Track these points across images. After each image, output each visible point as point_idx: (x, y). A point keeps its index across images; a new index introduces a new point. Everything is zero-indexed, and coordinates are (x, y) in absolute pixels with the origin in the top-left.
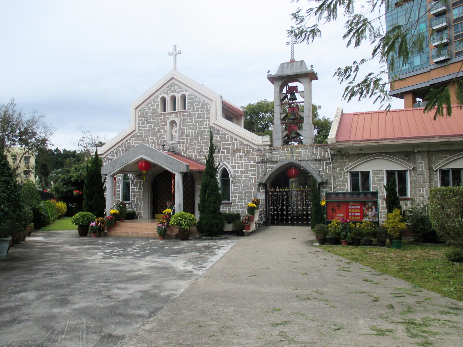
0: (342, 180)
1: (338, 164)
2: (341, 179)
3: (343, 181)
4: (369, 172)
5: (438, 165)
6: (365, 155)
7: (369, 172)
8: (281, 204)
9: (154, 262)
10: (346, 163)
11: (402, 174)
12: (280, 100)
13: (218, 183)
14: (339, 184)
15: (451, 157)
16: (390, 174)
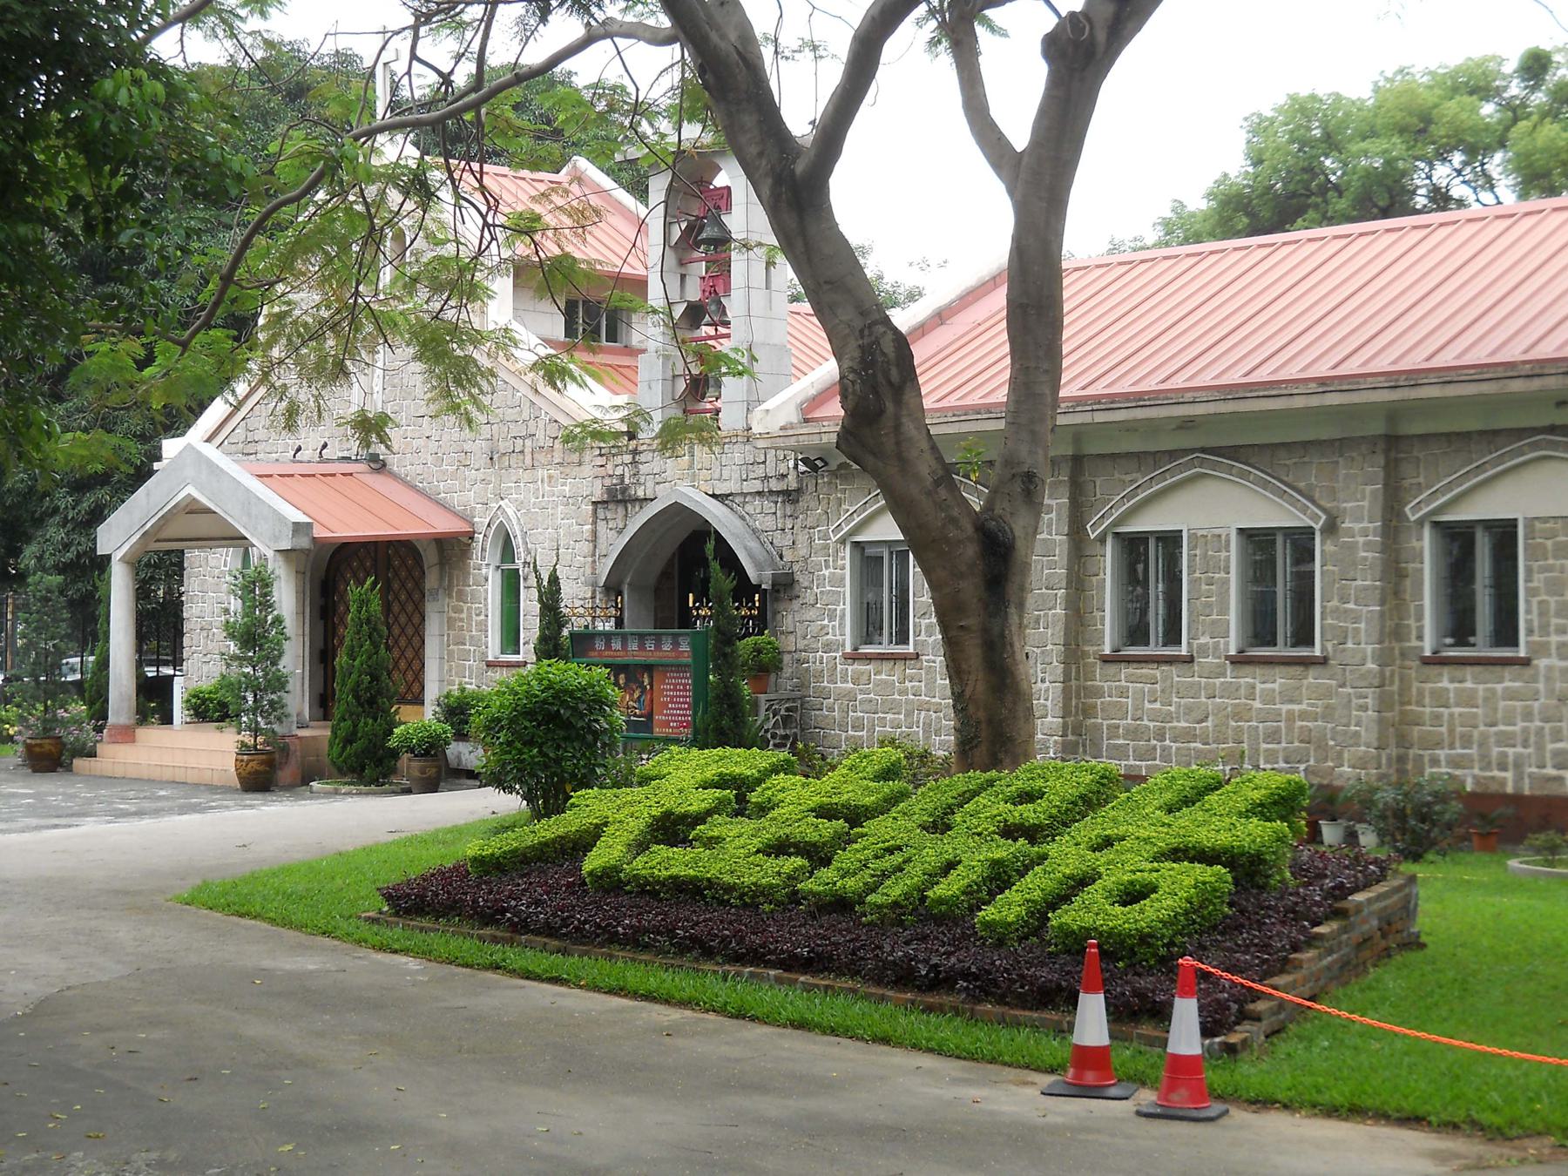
4: (1516, 520)
5: (1103, 516)
6: (1492, 437)
9: (483, 550)
11: (1301, 542)
15: (1144, 483)
16: (1257, 541)
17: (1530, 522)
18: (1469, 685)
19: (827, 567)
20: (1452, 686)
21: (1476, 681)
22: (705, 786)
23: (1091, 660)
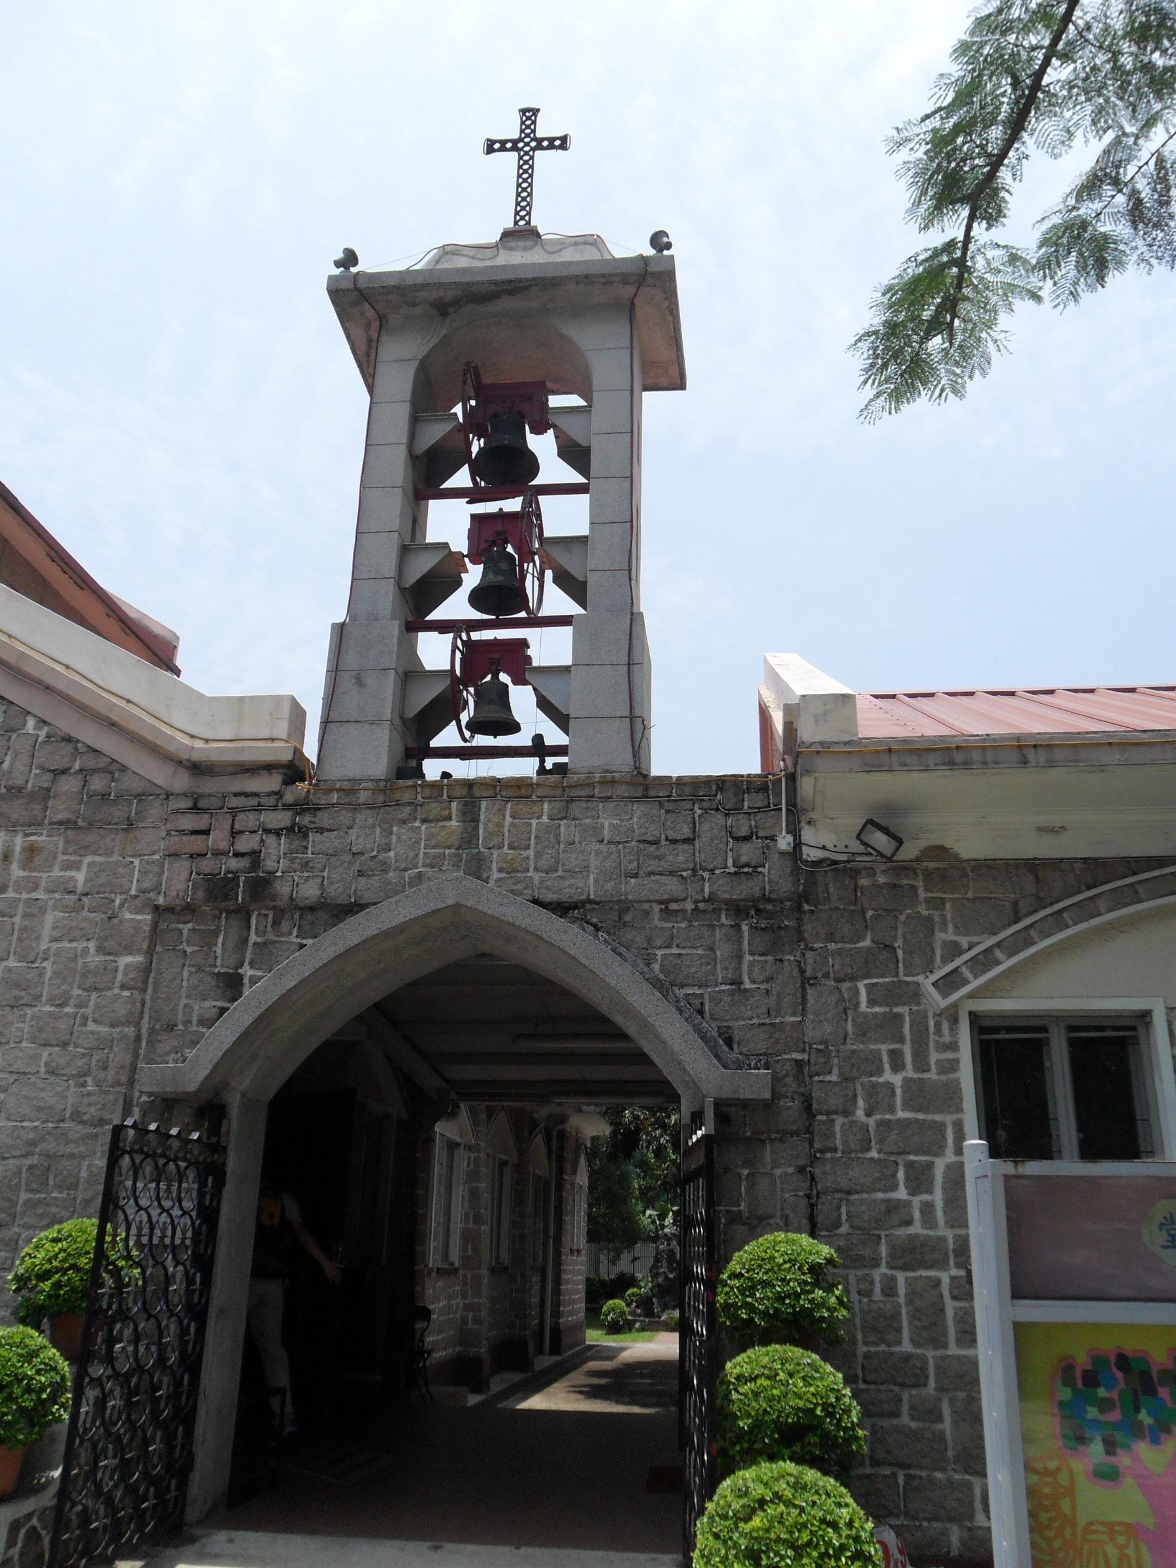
0: (906, 1081)
1: (867, 943)
2: (897, 1080)
3: (917, 1095)
4: (1144, 1016)
7: (1144, 1016)
8: (1024, 104)
10: (941, 936)
12: (413, 458)
13: (916, 1155)
14: (880, 1123)
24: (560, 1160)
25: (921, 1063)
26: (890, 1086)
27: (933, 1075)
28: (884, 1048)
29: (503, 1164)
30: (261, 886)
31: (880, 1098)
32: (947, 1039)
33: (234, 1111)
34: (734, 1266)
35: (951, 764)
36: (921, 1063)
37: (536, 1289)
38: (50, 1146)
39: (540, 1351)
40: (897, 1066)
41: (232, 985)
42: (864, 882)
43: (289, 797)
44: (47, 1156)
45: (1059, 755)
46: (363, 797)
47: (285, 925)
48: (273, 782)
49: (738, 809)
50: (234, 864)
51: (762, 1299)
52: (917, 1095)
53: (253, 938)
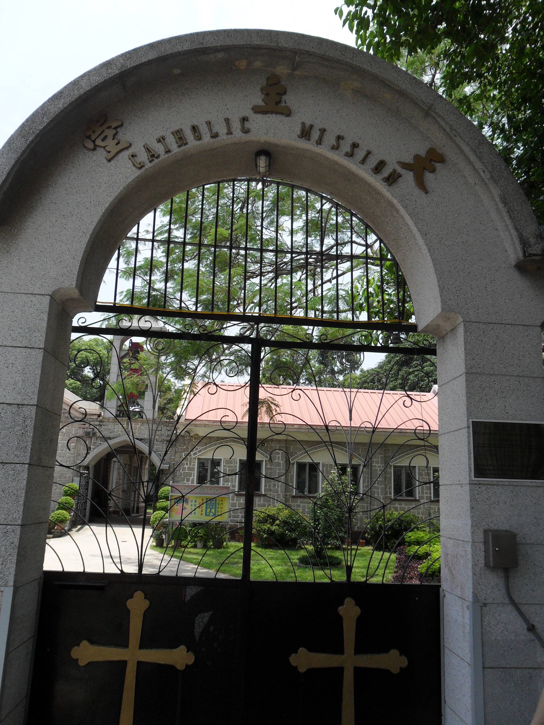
0: (188, 467)
2: (187, 467)
3: (189, 469)
17: (419, 467)
18: (403, 506)
19: (187, 465)
20: (399, 506)
21: (405, 505)
22: (344, 25)
23: (288, 497)
24: (141, 461)
25: (190, 465)
26: (186, 467)
27: (191, 466)
28: (185, 462)
29: (126, 464)
30: (94, 434)
31: (184, 469)
32: (194, 461)
33: (90, 467)
34: (160, 491)
35: (195, 426)
36: (190, 465)
37: (133, 496)
38: (62, 472)
39: (133, 513)
40: (187, 465)
41: (88, 449)
42: (185, 438)
43: (99, 420)
44: (61, 473)
45: (210, 426)
46: (111, 420)
47: (98, 440)
48: (96, 417)
49: (168, 426)
50: (90, 430)
51: (163, 495)
52: (189, 469)
53: (93, 441)
